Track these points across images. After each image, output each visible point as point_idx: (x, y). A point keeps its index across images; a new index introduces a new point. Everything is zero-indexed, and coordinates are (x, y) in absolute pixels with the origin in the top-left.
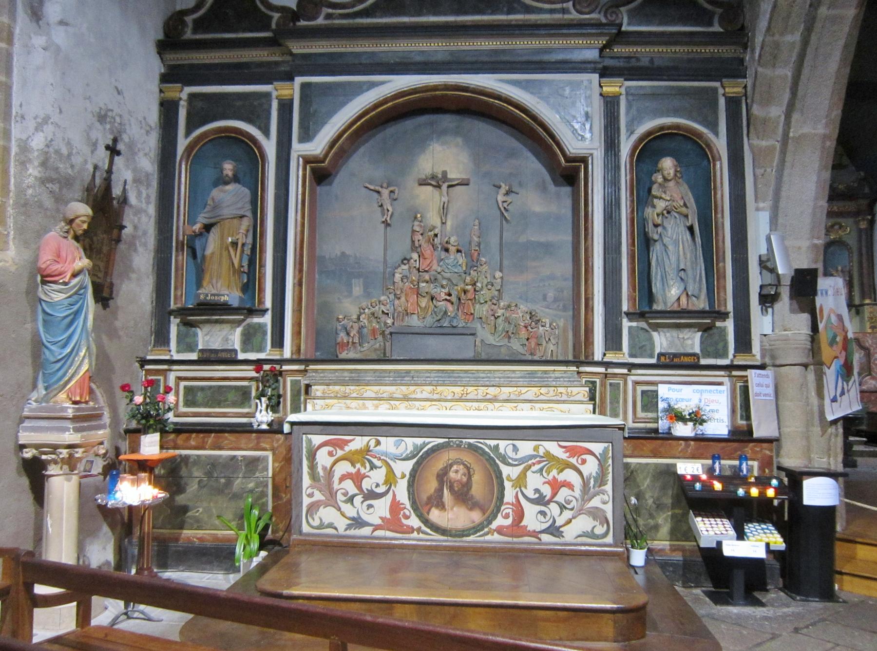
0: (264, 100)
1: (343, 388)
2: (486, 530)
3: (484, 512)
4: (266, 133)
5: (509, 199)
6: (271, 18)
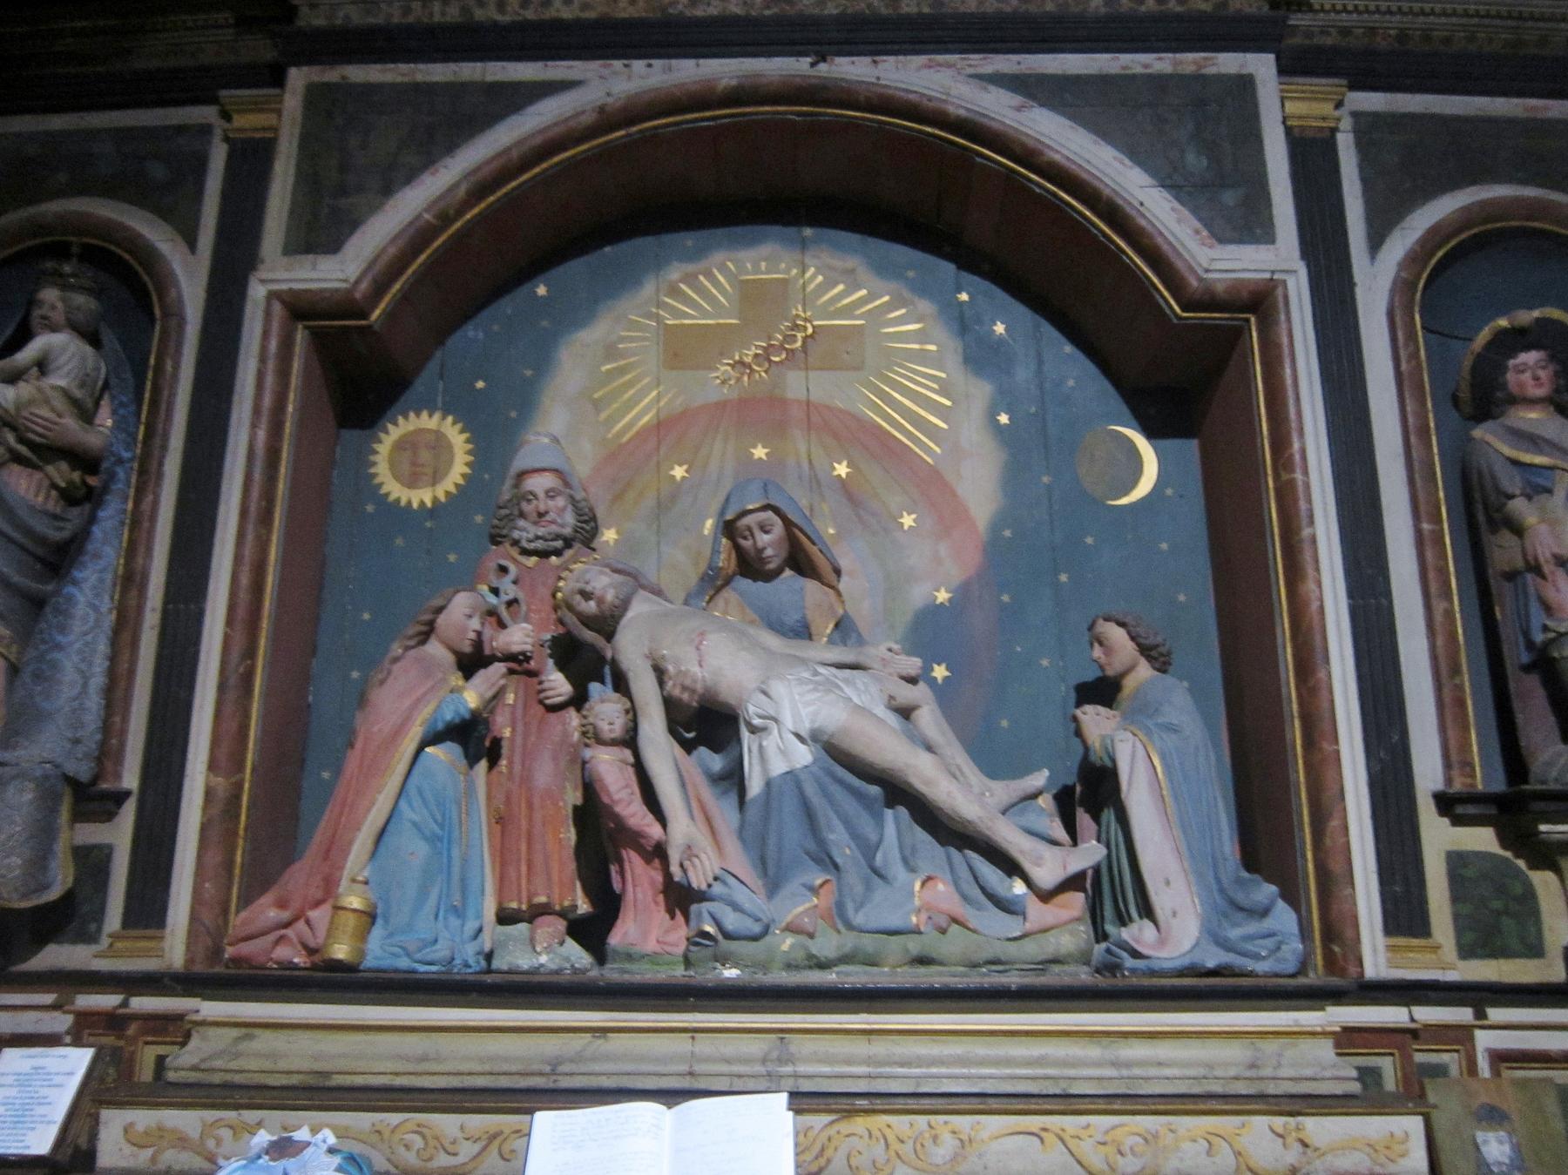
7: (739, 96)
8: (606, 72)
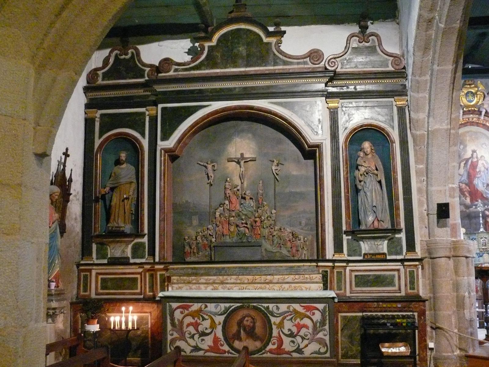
0: (141, 117)
1: (187, 278)
2: (263, 351)
3: (262, 341)
4: (143, 135)
5: (279, 168)
6: (144, 71)
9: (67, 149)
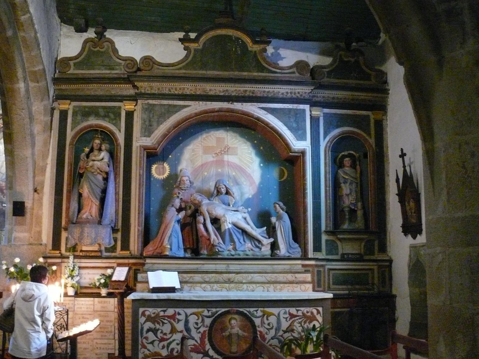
7: (220, 110)
8: (195, 104)
9: (402, 150)
